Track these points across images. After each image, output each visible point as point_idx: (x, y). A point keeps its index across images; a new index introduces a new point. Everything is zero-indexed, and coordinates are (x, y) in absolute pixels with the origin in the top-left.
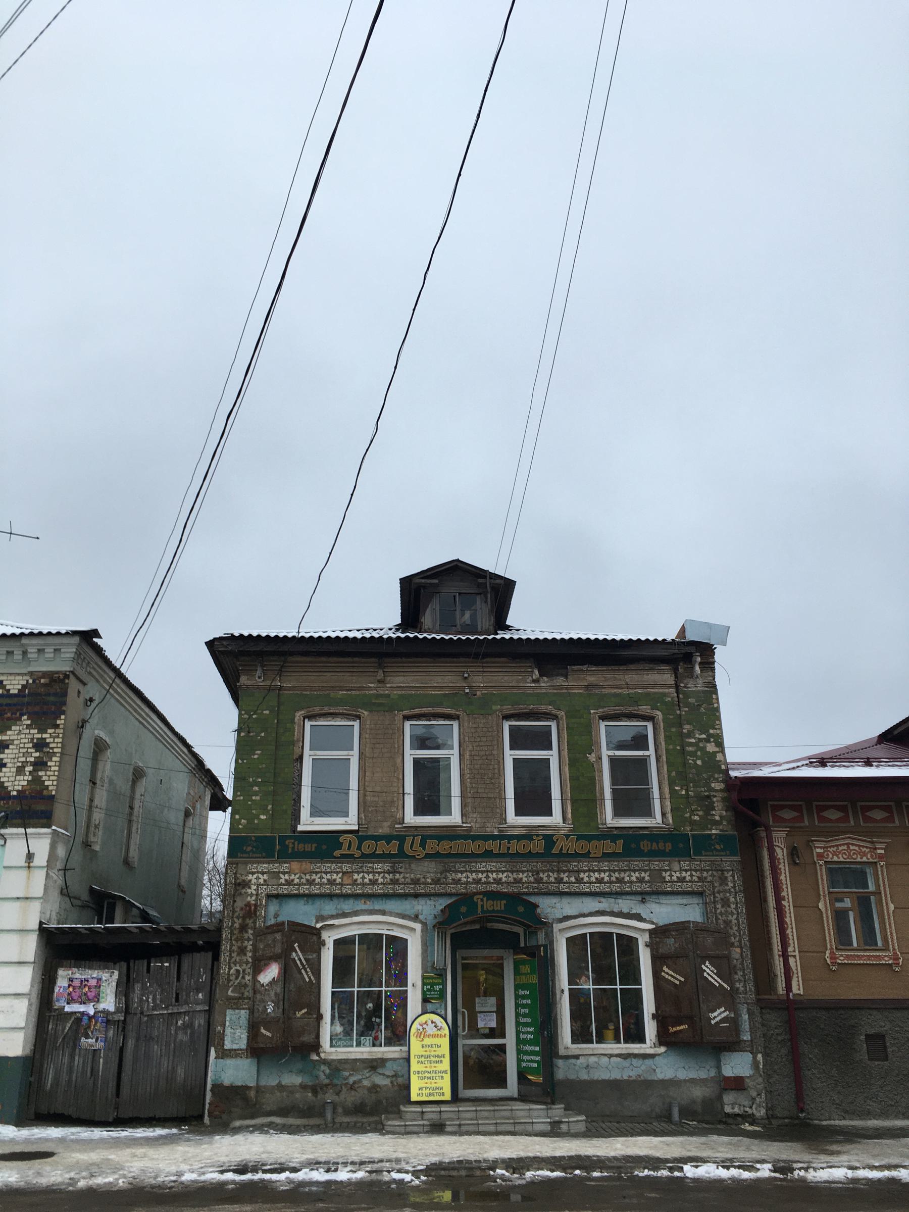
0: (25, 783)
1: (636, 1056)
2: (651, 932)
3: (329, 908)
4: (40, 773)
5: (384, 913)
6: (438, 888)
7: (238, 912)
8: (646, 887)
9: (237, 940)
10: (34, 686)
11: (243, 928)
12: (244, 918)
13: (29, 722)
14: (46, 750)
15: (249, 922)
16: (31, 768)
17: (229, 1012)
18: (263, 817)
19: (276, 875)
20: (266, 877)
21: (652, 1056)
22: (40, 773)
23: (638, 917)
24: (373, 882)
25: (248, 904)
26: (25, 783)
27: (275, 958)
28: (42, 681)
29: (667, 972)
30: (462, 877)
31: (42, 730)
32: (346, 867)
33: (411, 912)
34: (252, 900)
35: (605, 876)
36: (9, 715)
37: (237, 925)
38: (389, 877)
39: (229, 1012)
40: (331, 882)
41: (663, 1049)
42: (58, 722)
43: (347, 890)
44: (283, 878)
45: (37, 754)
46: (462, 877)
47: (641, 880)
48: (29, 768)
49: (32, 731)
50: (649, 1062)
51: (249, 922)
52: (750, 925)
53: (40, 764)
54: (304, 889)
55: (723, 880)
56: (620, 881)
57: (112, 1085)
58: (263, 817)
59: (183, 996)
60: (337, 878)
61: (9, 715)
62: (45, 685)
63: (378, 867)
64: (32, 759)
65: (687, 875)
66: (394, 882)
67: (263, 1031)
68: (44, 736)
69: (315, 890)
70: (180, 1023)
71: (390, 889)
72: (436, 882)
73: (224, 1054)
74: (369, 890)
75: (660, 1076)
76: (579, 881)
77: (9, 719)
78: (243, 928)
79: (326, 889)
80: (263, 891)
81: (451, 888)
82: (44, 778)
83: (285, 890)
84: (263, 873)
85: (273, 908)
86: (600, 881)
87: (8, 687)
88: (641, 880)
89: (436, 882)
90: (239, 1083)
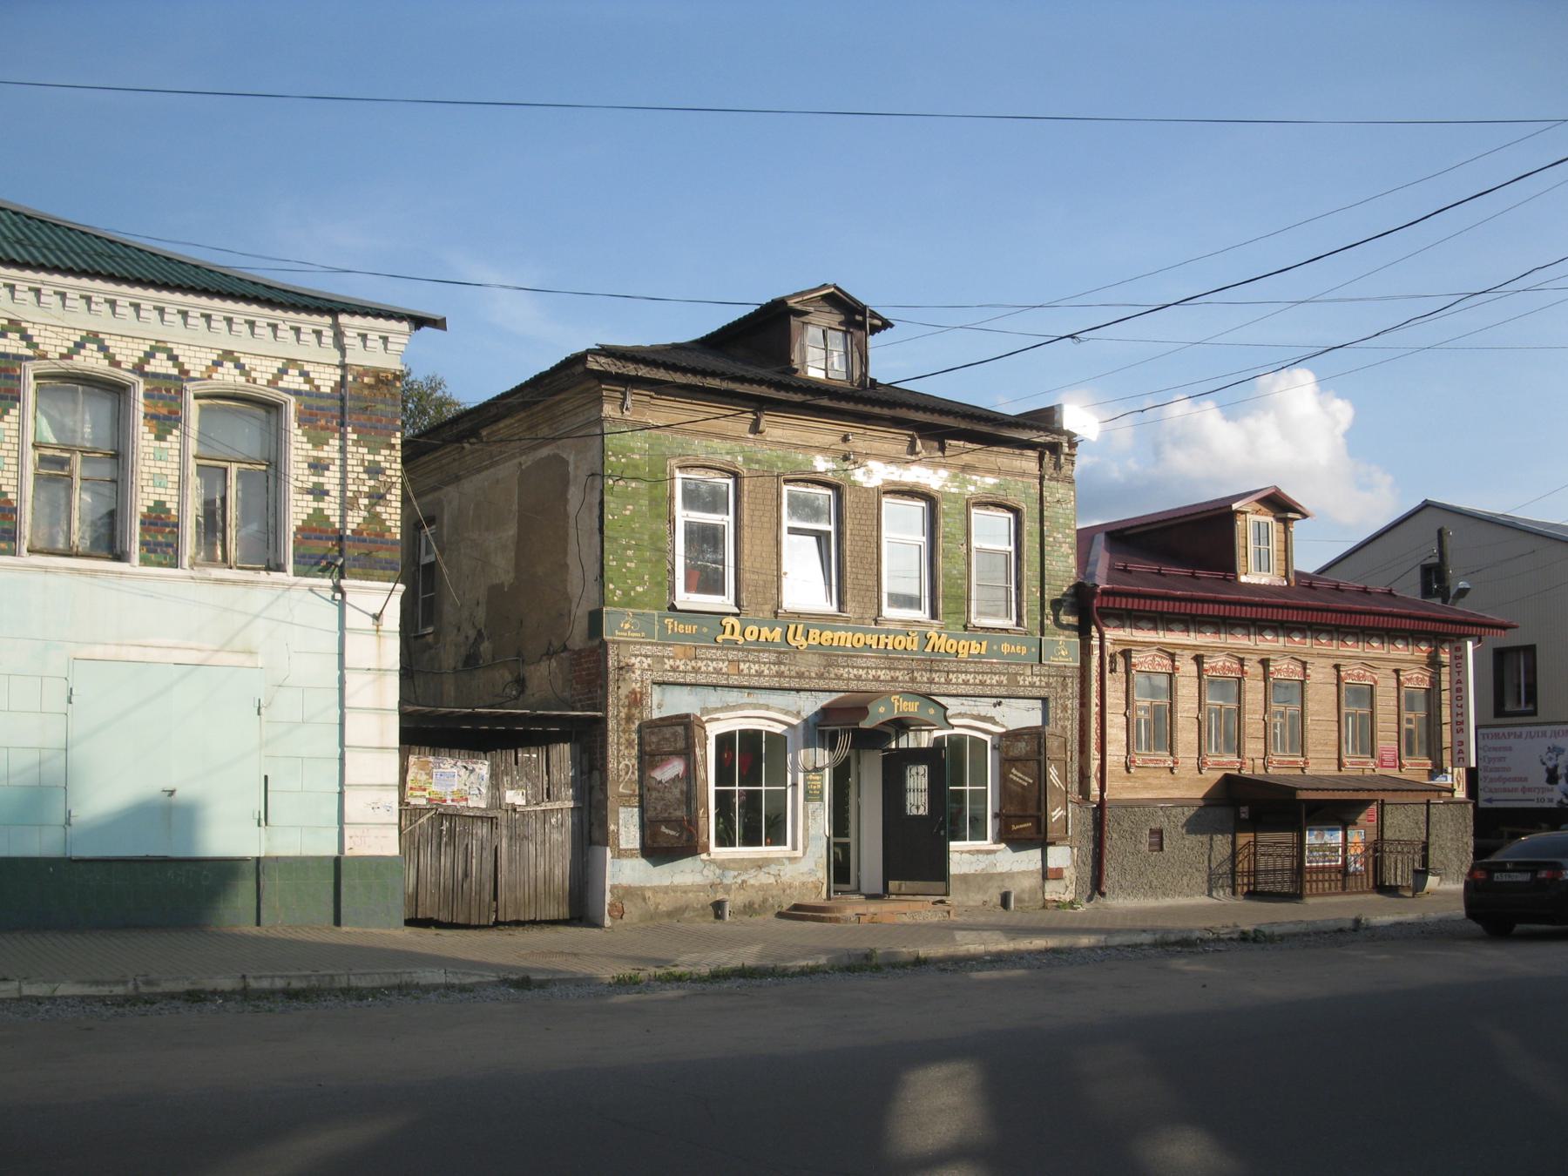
0: (360, 520)
1: (979, 852)
2: (1001, 735)
3: (714, 698)
4: (379, 509)
5: (768, 708)
6: (822, 684)
7: (624, 701)
8: (1003, 691)
9: (624, 731)
10: (356, 385)
11: (629, 719)
12: (629, 706)
13: (355, 437)
14: (382, 478)
15: (636, 712)
16: (366, 501)
17: (621, 810)
18: (639, 589)
19: (660, 659)
20: (649, 661)
21: (994, 852)
22: (379, 509)
23: (992, 720)
24: (760, 674)
25: (633, 692)
26: (360, 520)
27: (676, 753)
28: (366, 380)
29: (1016, 775)
30: (843, 672)
31: (374, 450)
32: (732, 655)
33: (794, 709)
34: (637, 686)
35: (970, 677)
36: (323, 422)
37: (623, 715)
38: (775, 668)
39: (621, 810)
40: (718, 672)
41: (1003, 846)
42: (393, 441)
43: (734, 680)
44: (669, 663)
45: (372, 483)
46: (843, 672)
47: (1000, 684)
48: (364, 501)
49: (361, 450)
50: (991, 857)
51: (636, 712)
52: (1497, 810)
53: (377, 497)
54: (690, 678)
55: (1064, 687)
56: (982, 683)
57: (488, 887)
58: (639, 589)
59: (554, 790)
60: (723, 666)
61: (323, 422)
62: (370, 386)
63: (765, 657)
64: (366, 489)
65: (1036, 679)
66: (780, 675)
67: (663, 829)
68: (378, 458)
69: (702, 679)
70: (553, 821)
71: (775, 682)
72: (820, 676)
73: (620, 854)
74: (755, 682)
75: (999, 870)
76: (948, 682)
77: (323, 428)
78: (629, 719)
79: (713, 679)
80: (648, 676)
81: (834, 685)
82: (384, 516)
83: (671, 677)
84: (646, 656)
85: (656, 695)
86: (966, 683)
87: (317, 382)
88: (1000, 684)
89: (820, 676)
90: (636, 884)
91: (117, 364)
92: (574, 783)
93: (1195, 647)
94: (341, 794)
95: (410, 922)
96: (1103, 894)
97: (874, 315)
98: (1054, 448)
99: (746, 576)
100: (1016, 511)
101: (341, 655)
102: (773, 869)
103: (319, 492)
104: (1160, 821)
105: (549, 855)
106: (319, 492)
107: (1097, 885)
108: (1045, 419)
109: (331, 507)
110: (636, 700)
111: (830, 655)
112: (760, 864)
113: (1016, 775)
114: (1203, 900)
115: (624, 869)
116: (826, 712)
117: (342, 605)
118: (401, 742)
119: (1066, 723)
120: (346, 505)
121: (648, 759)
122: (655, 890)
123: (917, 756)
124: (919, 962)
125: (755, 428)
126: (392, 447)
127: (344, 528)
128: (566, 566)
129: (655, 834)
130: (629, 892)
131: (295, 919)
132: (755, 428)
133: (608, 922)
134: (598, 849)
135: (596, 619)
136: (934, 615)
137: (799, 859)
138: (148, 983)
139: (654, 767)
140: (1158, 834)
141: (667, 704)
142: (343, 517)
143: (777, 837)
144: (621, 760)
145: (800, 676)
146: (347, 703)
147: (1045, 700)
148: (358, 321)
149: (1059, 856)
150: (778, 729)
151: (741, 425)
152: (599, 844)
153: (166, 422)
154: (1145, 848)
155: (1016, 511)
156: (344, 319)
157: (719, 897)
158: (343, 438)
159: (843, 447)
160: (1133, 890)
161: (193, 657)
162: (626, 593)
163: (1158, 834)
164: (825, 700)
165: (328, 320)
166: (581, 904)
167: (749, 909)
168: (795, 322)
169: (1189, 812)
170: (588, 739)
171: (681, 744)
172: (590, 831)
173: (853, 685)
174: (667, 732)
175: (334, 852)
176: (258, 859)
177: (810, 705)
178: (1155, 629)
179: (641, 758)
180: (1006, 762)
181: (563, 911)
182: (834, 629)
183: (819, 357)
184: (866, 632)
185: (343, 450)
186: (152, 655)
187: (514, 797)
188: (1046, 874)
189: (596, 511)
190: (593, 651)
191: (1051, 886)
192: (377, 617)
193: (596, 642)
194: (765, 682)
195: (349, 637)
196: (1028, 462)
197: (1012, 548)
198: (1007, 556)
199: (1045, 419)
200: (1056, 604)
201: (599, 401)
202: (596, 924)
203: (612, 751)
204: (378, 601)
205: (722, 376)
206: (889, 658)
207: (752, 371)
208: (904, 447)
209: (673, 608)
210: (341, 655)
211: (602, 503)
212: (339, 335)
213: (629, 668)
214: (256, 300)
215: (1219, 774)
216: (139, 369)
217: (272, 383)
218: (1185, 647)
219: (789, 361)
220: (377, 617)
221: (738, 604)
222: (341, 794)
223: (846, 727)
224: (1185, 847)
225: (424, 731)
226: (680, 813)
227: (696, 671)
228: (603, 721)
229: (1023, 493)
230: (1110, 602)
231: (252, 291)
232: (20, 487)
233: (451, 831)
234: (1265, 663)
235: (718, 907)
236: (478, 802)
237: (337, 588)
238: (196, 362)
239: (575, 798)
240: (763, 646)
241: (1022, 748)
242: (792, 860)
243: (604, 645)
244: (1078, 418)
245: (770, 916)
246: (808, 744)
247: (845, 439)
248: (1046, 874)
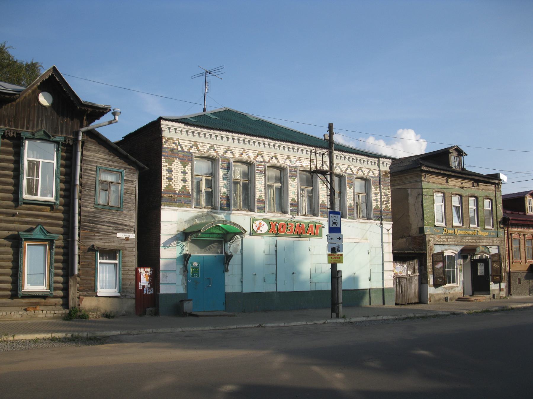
5: (452, 250)
6: (461, 244)
11: (430, 253)
66: (454, 242)
72: (461, 242)
73: (430, 286)
89: (461, 242)
91: (342, 171)
92: (419, 269)
93: (523, 232)
94: (383, 273)
95: (396, 304)
96: (511, 295)
97: (465, 153)
98: (498, 184)
99: (447, 218)
100: (491, 200)
101: (382, 239)
102: (454, 289)
103: (184, 181)
104: (520, 276)
105: (414, 287)
106: (376, 201)
107: (509, 293)
108: (496, 176)
109: (379, 204)
110: (431, 249)
111: (463, 236)
112: (452, 288)
113: (495, 265)
114: (528, 296)
115: (431, 290)
116: (462, 250)
117: (382, 228)
118: (393, 260)
119: (504, 252)
120: (382, 203)
121: (434, 263)
122: (436, 294)
123: (480, 260)
124: (512, 309)
125: (447, 182)
126: (389, 189)
127: (381, 209)
128: (409, 216)
129: (437, 281)
130: (432, 295)
131: (376, 302)
132: (447, 182)
133: (428, 302)
134: (425, 285)
135: (422, 230)
136: (478, 226)
137: (457, 287)
138: (401, 316)
139: (436, 265)
140: (520, 279)
141: (437, 249)
142: (381, 206)
143: (454, 282)
144: (429, 263)
145: (458, 242)
146: (384, 251)
147: (498, 246)
148: (167, 123)
149: (503, 285)
150: (453, 255)
151: (442, 180)
152: (424, 283)
153: (352, 184)
154: (517, 283)
155: (491, 200)
156: (380, 159)
157: (446, 296)
158: (380, 187)
159: (461, 186)
160: (519, 294)
161: (357, 241)
162: (428, 222)
163: (520, 279)
164: (462, 247)
165: (377, 159)
166: (422, 298)
167: (451, 299)
168: (450, 155)
169: (525, 274)
170: (422, 259)
171: (442, 259)
172: (423, 280)
173: (467, 244)
174: (439, 256)
175: (381, 287)
176: (370, 289)
177: (459, 248)
178: (518, 228)
179: (433, 263)
180: (493, 262)
181: (416, 300)
182: (462, 230)
183: (454, 162)
184: (468, 230)
185: (380, 190)
186: (351, 240)
187: (410, 273)
188: (501, 290)
189: (420, 203)
190: (421, 237)
191: (501, 293)
192: (388, 230)
193: (422, 235)
194: (452, 243)
195: (384, 235)
196: (492, 187)
197: (460, 205)
198: (489, 211)
199: (496, 176)
200: (500, 222)
201: (421, 176)
202: (425, 303)
203: (428, 261)
204: (388, 225)
205: (435, 168)
206: (472, 236)
207: (439, 167)
208: (471, 185)
209: (435, 226)
210: (382, 239)
211: (422, 201)
212: (379, 162)
213: (429, 241)
214: (343, 151)
215: (529, 264)
216: (345, 172)
217: (368, 175)
218: (528, 233)
219: (449, 165)
220: (388, 230)
221: (446, 224)
222: (383, 273)
223: (466, 253)
224: (524, 282)
225: (398, 258)
226: (442, 276)
227: (441, 241)
228: (426, 254)
229: (492, 194)
230: (513, 222)
231: (354, 151)
232: (192, 189)
233: (399, 281)
234: (524, 235)
235: (446, 299)
236: (404, 274)
237: (381, 224)
238: (355, 170)
239: (419, 272)
240: (451, 235)
241: (496, 258)
242: (457, 287)
243: (425, 235)
244: (503, 177)
245: (454, 301)
246: (459, 258)
247: (462, 184)
248: (501, 290)
